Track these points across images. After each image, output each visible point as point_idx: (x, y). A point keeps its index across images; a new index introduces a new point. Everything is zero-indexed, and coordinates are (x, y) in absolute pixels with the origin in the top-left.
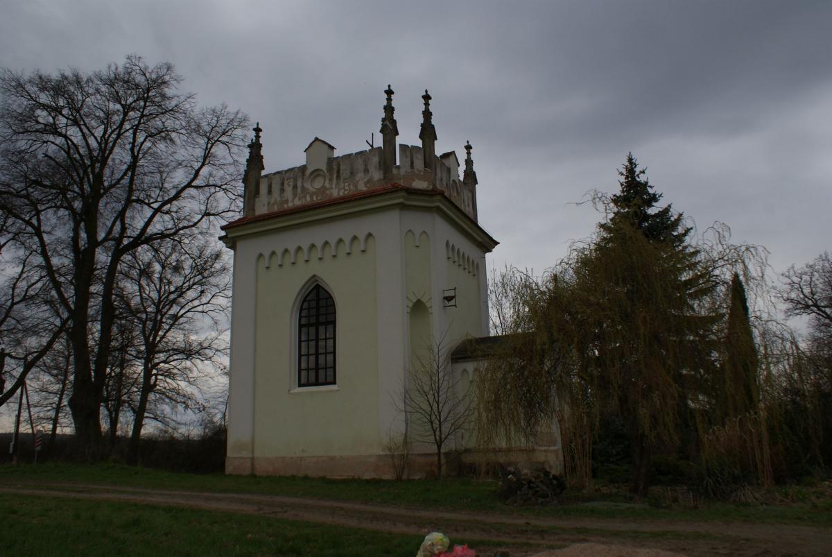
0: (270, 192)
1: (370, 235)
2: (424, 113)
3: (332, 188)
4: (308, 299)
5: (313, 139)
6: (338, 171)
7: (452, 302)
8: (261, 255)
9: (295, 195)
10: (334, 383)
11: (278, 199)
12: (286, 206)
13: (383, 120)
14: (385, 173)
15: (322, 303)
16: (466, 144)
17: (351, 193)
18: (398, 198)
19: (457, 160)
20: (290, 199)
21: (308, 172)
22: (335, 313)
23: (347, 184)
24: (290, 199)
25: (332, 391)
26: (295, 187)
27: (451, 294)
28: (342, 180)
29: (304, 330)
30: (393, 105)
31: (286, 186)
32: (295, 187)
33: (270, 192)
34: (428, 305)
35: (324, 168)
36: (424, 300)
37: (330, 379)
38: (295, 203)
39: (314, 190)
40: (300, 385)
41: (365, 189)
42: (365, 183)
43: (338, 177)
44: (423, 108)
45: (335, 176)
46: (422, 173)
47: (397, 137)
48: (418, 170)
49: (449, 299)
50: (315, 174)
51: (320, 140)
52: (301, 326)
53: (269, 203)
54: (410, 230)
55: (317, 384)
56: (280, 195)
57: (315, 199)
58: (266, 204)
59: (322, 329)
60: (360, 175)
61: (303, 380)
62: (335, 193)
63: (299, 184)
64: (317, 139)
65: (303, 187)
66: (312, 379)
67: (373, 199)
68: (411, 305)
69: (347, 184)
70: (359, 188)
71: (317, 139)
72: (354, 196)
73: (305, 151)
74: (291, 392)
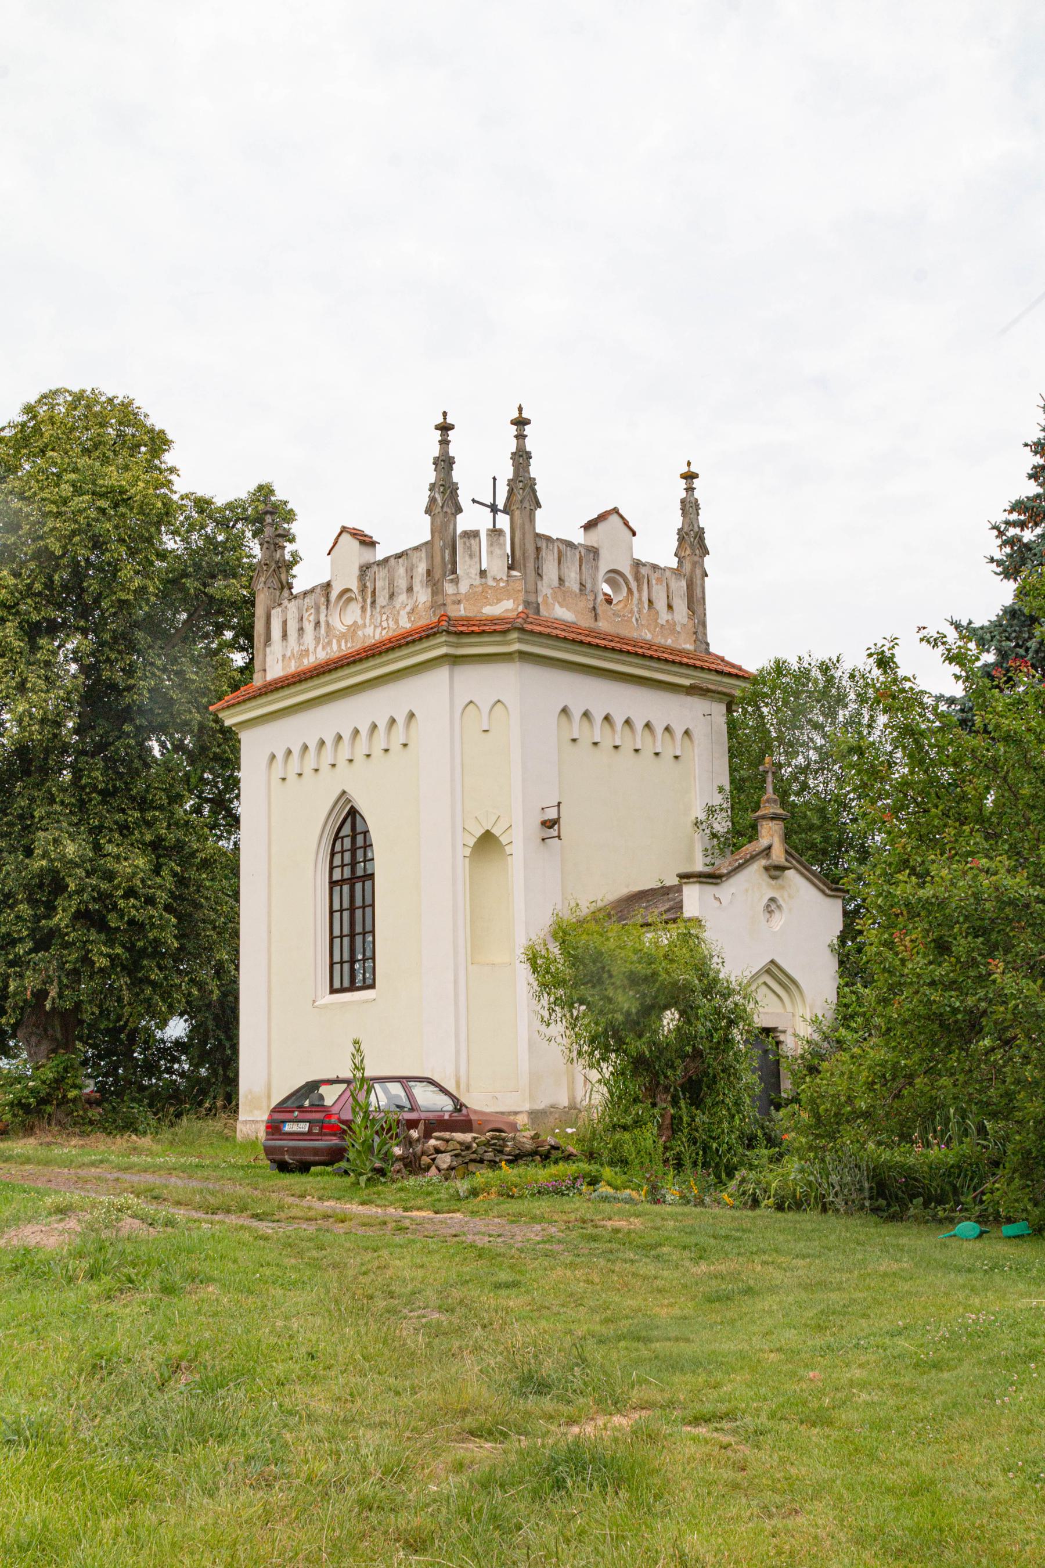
0: (285, 636)
1: (412, 715)
2: (515, 456)
3: (365, 625)
4: (341, 834)
5: (339, 531)
6: (374, 593)
7: (554, 832)
8: (273, 757)
9: (317, 639)
10: (372, 986)
11: (296, 649)
12: (305, 661)
13: (432, 488)
14: (434, 594)
15: (360, 840)
16: (685, 469)
17: (391, 634)
18: (439, 646)
19: (626, 524)
20: (311, 648)
21: (334, 595)
22: (236, 896)
23: (384, 617)
24: (311, 648)
25: (366, 1001)
26: (317, 624)
27: (552, 814)
28: (378, 609)
29: (337, 889)
30: (451, 454)
31: (306, 624)
32: (317, 624)
33: (285, 636)
34: (504, 840)
35: (354, 585)
36: (496, 831)
37: (369, 982)
38: (318, 656)
39: (343, 629)
40: (333, 991)
41: (408, 626)
42: (408, 613)
43: (373, 602)
44: (512, 446)
45: (369, 601)
46: (502, 584)
47: (459, 517)
48: (494, 579)
49: (549, 824)
50: (345, 597)
51: (621, 517)
52: (333, 884)
53: (284, 656)
54: (471, 702)
55: (352, 988)
56: (299, 640)
57: (343, 647)
58: (280, 658)
59: (359, 886)
60: (402, 598)
61: (337, 985)
62: (373, 633)
63: (322, 619)
64: (616, 511)
65: (328, 624)
66: (346, 984)
67: (405, 651)
68: (471, 842)
69: (384, 617)
70: (401, 624)
71: (344, 530)
72: (327, 663)
73: (329, 554)
74: (316, 1004)
